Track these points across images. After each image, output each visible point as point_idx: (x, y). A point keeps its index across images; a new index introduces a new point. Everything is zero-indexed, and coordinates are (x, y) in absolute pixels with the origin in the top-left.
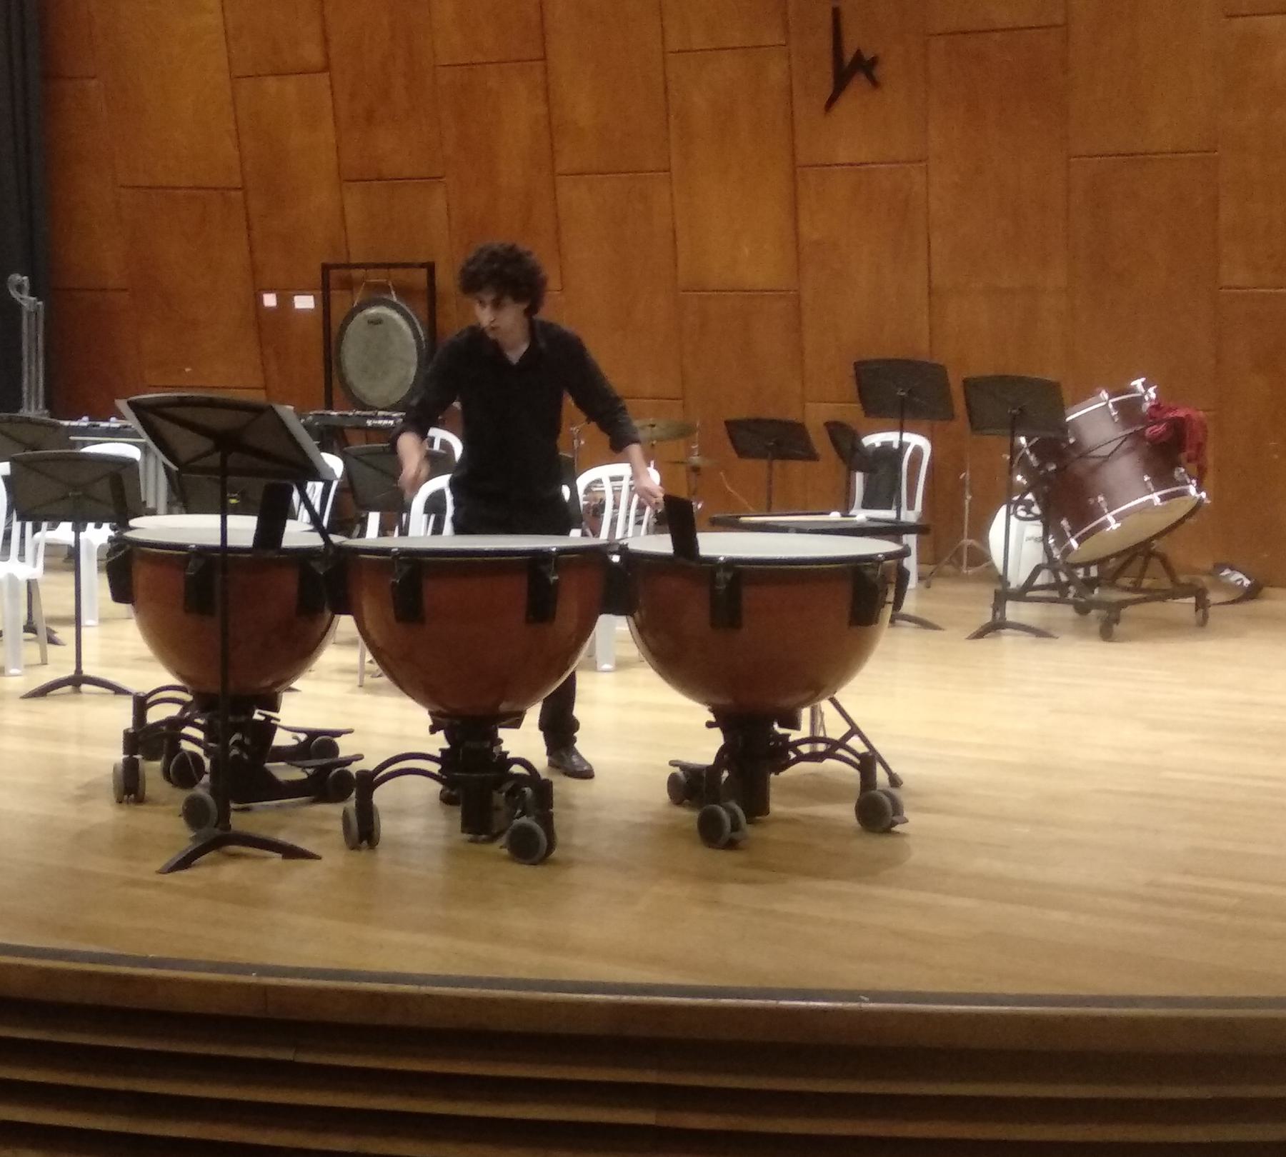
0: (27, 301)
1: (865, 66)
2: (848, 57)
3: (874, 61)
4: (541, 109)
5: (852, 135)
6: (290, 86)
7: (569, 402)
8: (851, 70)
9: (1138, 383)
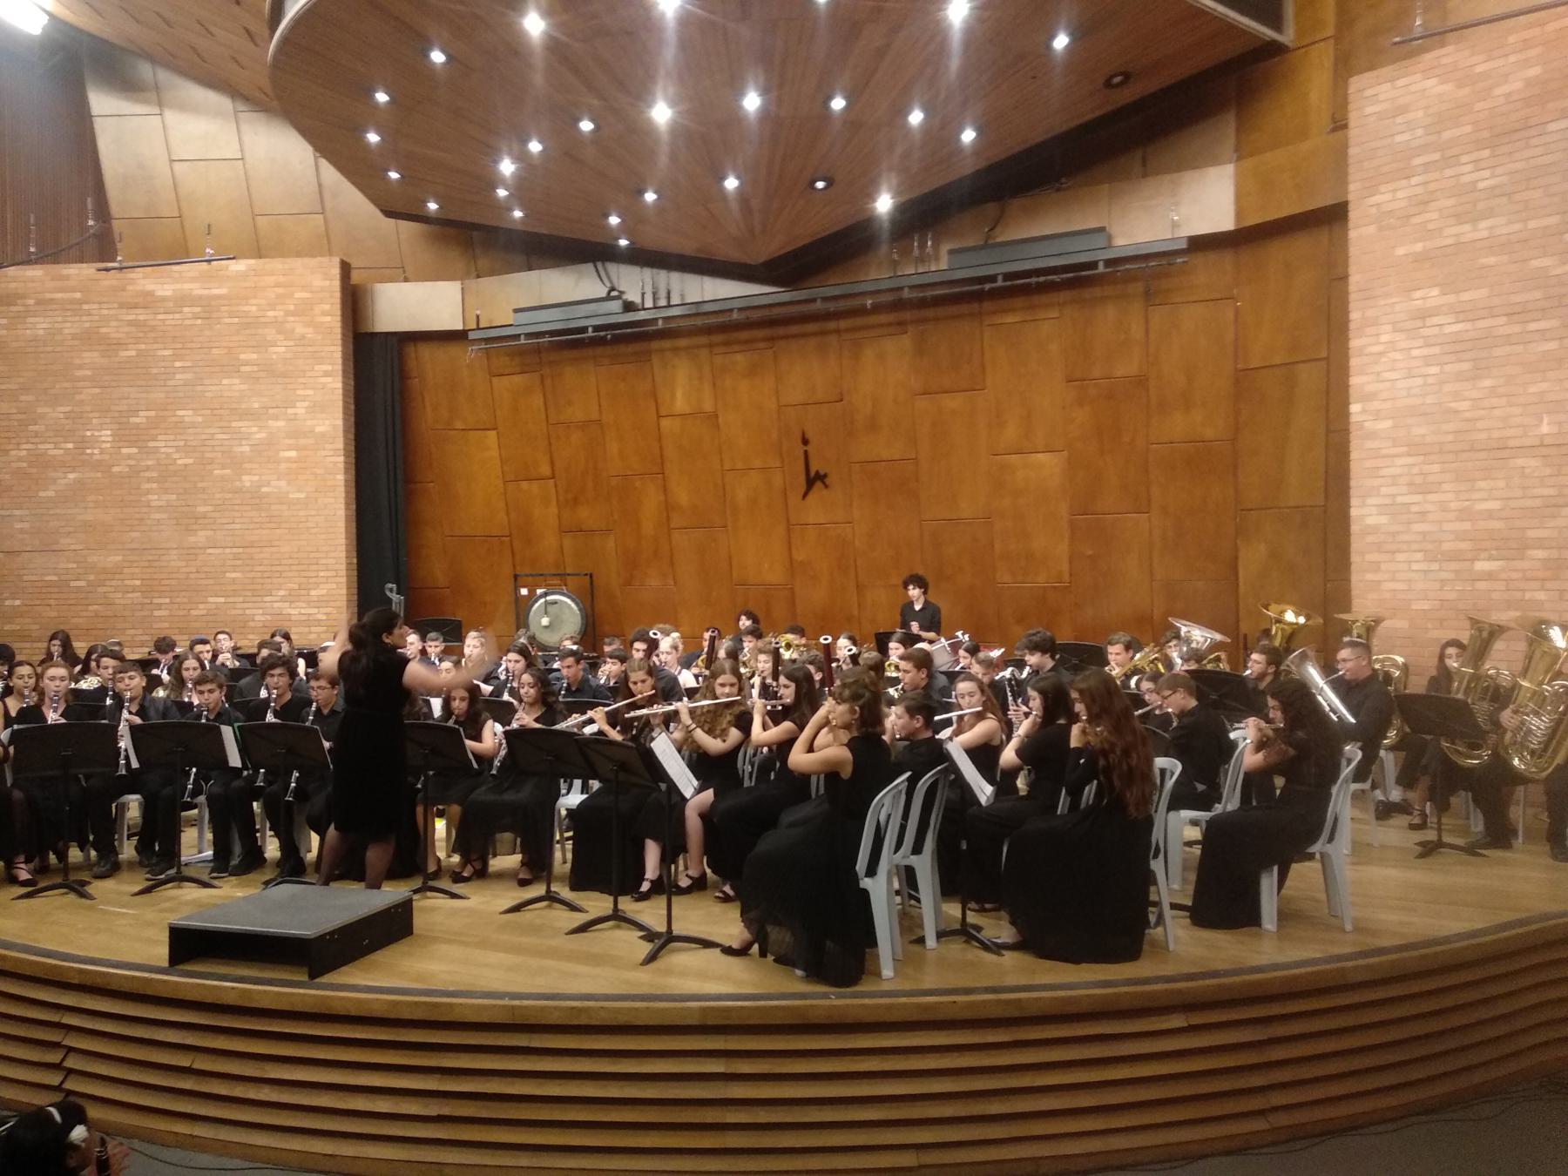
0: (395, 597)
1: (821, 478)
2: (813, 474)
3: (825, 476)
4: (662, 498)
5: (816, 509)
6: (535, 487)
7: (1218, 637)
8: (814, 480)
9: (959, 634)
